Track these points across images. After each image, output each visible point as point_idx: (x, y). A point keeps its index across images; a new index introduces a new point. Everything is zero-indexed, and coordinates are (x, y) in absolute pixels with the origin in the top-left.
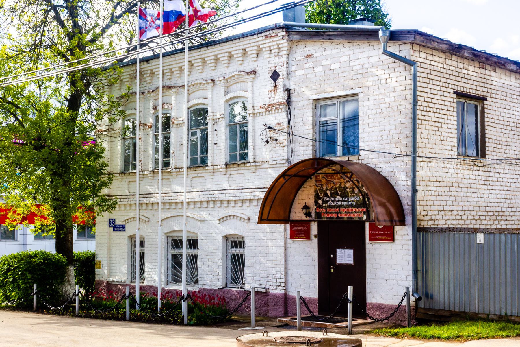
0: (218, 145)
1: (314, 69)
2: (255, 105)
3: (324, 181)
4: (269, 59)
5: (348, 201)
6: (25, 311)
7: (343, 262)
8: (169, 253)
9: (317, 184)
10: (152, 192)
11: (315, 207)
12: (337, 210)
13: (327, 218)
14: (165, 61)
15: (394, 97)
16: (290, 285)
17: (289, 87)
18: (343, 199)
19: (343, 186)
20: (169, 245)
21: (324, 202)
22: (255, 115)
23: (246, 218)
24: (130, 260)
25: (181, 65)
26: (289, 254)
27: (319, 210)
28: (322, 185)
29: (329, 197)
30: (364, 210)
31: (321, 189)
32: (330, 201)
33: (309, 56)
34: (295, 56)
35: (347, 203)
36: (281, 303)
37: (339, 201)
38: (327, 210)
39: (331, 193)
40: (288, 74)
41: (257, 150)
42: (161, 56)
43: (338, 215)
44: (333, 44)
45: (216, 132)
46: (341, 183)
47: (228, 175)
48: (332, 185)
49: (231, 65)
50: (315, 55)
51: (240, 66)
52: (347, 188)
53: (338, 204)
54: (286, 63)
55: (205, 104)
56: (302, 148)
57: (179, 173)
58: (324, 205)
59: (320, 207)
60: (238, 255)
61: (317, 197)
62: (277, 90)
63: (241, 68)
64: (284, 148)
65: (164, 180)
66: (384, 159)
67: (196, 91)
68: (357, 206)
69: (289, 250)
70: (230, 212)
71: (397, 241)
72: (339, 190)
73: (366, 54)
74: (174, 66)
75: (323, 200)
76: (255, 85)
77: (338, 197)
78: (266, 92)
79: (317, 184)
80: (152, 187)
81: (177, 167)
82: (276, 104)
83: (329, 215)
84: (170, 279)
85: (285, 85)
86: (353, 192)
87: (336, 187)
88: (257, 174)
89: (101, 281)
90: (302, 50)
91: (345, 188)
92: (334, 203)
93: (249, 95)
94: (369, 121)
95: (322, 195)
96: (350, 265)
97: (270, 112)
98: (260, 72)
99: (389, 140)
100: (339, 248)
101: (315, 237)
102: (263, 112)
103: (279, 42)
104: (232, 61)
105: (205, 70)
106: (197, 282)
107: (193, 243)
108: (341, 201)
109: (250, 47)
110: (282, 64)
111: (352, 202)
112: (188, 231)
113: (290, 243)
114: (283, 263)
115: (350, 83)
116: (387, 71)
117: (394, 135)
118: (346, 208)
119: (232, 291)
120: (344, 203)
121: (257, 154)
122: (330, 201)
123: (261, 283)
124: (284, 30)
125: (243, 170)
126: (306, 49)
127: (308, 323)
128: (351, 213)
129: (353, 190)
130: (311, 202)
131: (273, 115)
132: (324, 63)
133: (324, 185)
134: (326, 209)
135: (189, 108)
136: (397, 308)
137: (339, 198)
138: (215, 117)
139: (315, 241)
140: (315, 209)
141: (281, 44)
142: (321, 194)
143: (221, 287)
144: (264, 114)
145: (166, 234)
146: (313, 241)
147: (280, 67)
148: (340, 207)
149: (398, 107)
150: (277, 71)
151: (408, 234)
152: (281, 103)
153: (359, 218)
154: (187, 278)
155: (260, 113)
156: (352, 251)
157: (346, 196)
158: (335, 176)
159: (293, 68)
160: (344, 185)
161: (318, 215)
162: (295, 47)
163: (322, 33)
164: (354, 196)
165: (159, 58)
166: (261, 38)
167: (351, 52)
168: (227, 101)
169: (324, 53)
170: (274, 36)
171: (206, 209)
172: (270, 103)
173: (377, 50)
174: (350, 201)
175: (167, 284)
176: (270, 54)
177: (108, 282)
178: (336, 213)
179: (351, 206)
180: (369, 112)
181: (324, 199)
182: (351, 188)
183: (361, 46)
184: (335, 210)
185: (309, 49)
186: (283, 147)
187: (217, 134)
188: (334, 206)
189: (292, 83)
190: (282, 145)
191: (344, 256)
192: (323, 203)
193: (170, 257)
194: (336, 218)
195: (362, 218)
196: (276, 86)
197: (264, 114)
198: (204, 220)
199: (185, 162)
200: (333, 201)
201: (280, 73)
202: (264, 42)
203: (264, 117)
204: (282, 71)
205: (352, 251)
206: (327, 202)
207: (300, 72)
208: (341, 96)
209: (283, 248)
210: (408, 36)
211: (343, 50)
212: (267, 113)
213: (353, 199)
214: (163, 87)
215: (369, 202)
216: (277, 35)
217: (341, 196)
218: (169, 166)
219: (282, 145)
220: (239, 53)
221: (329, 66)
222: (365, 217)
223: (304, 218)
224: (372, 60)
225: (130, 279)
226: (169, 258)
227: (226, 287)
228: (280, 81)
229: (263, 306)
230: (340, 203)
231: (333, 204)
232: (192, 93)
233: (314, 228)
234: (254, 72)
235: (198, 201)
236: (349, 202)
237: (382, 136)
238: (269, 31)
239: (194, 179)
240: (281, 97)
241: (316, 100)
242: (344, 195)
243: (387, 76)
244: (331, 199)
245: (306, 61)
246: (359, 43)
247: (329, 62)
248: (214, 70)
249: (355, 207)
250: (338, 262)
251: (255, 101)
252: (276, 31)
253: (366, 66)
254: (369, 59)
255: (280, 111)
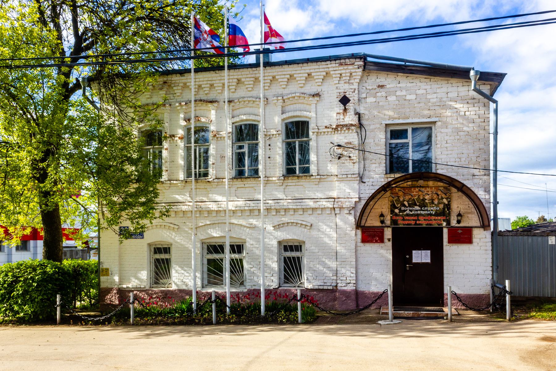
0: (272, 159)
1: (387, 98)
2: (318, 125)
3: (401, 193)
4: (337, 85)
5: (427, 210)
6: (47, 325)
7: (419, 261)
8: (204, 258)
9: (393, 196)
10: (182, 201)
11: (391, 215)
12: (416, 218)
13: (404, 225)
14: (197, 77)
15: (473, 127)
16: (360, 282)
17: (358, 111)
18: (421, 208)
19: (422, 198)
20: (204, 250)
21: (400, 211)
22: (319, 134)
23: (309, 225)
24: (149, 266)
25: (212, 82)
26: (359, 255)
27: (395, 218)
28: (398, 197)
29: (407, 207)
30: (444, 218)
31: (398, 200)
32: (408, 211)
33: (381, 87)
34: (365, 85)
35: (426, 212)
36: (353, 297)
37: (417, 210)
38: (404, 218)
39: (408, 204)
40: (359, 100)
41: (320, 165)
42: (193, 71)
43: (416, 222)
44: (408, 78)
45: (269, 147)
46: (419, 196)
47: (284, 187)
48: (410, 197)
49: (288, 87)
50: (388, 86)
51: (301, 89)
52: (426, 199)
53: (416, 212)
54: (357, 90)
55: (306, 117)
56: (374, 165)
57: (220, 184)
58: (401, 214)
59: (396, 215)
60: (294, 258)
61: (393, 207)
62: (346, 113)
63: (302, 90)
64: (355, 164)
65: (198, 190)
66: (462, 177)
67: (242, 108)
68: (437, 214)
69: (359, 252)
70: (285, 219)
71: (475, 244)
72: (417, 201)
73: (445, 90)
74: (217, 82)
75: (400, 210)
76: (318, 107)
77: (416, 207)
78: (335, 115)
79: (393, 196)
80: (182, 196)
81: (217, 177)
82: (347, 126)
83: (407, 222)
84: (206, 282)
85: (355, 110)
86: (433, 203)
87: (414, 199)
88: (320, 186)
89: (110, 288)
90: (373, 80)
91: (424, 200)
92: (411, 212)
93: (313, 114)
94: (447, 145)
95: (399, 205)
96: (427, 263)
97: (339, 132)
98: (325, 96)
99: (467, 162)
100: (415, 250)
101: (389, 240)
102: (328, 132)
103: (353, 71)
104: (290, 84)
105: (255, 89)
106: (242, 284)
107: (237, 248)
108: (419, 210)
109: (318, 72)
110: (353, 90)
111: (431, 212)
112: (231, 237)
113: (360, 247)
114: (354, 263)
115: (426, 112)
116: (466, 106)
117: (472, 158)
118: (424, 216)
119: (290, 290)
120: (423, 212)
121: (320, 168)
122: (408, 211)
123: (325, 281)
124: (362, 60)
125: (304, 182)
126: (378, 80)
127: (416, 313)
128: (431, 220)
129: (432, 201)
130: (386, 210)
131: (342, 135)
132: (398, 93)
133: (401, 197)
134: (403, 217)
135: (233, 123)
136: (381, 295)
137: (417, 208)
138: (269, 133)
139: (390, 244)
140: (391, 217)
141: (355, 72)
142: (398, 204)
143: (277, 287)
144: (330, 133)
145: (201, 240)
146: (386, 244)
147: (351, 93)
148: (418, 215)
149: (477, 135)
150: (347, 96)
151: (486, 238)
152: (352, 125)
153: (439, 225)
154: (231, 281)
155: (324, 132)
156: (429, 251)
157: (425, 207)
158: (412, 190)
159: (364, 95)
160: (423, 197)
161: (394, 222)
162: (365, 78)
163: (404, 67)
164: (433, 207)
165: (191, 72)
166: (334, 65)
167: (428, 87)
168: (283, 120)
169: (399, 85)
170: (350, 64)
171: (258, 217)
172: (339, 124)
173: (456, 87)
174: (429, 211)
175: (203, 287)
176: (339, 81)
177: (119, 288)
178: (413, 220)
179: (431, 215)
180: (446, 138)
181: (401, 208)
182: (430, 200)
183: (438, 83)
184: (413, 218)
185: (382, 80)
186: (354, 163)
187: (270, 149)
188: (411, 214)
189: (362, 108)
190: (353, 161)
191: (420, 256)
192: (399, 212)
193: (205, 262)
194: (414, 225)
195: (442, 225)
196: (345, 110)
197: (330, 133)
198: (254, 226)
199: (228, 172)
200: (411, 211)
201: (350, 99)
202: (337, 69)
203: (329, 136)
204: (353, 97)
205: (429, 251)
206: (405, 211)
207: (370, 100)
208: (413, 123)
209: (354, 251)
210: (495, 78)
211: (419, 84)
212: (336, 132)
213: (432, 209)
214: (196, 101)
215: (449, 211)
216: (353, 64)
217: (419, 206)
218: (208, 176)
219: (353, 161)
220: (303, 77)
221: (404, 97)
222: (444, 224)
223: (378, 224)
224: (450, 95)
225: (149, 285)
226: (204, 263)
227: (280, 286)
228: (350, 106)
229: (329, 301)
230: (419, 212)
231: (411, 213)
232: (236, 109)
233: (388, 233)
234: (318, 95)
235: (292, 209)
236: (428, 211)
237: (460, 158)
238: (345, 59)
239: (239, 189)
240: (350, 118)
241: (386, 125)
242: (423, 205)
243: (467, 109)
244: (408, 209)
245: (378, 90)
246: (437, 80)
247: (404, 93)
248: (284, 88)
249: (434, 215)
250: (414, 260)
251: (319, 122)
252: (353, 60)
253: (444, 99)
254: (447, 94)
255: (351, 131)
